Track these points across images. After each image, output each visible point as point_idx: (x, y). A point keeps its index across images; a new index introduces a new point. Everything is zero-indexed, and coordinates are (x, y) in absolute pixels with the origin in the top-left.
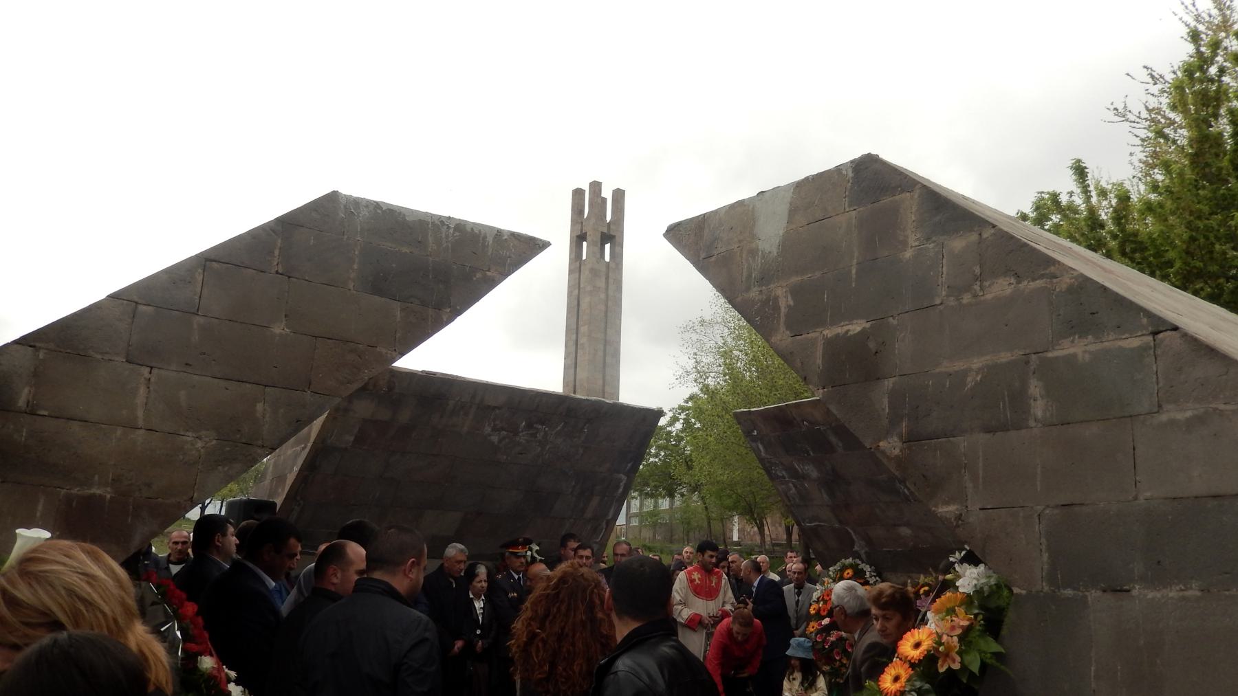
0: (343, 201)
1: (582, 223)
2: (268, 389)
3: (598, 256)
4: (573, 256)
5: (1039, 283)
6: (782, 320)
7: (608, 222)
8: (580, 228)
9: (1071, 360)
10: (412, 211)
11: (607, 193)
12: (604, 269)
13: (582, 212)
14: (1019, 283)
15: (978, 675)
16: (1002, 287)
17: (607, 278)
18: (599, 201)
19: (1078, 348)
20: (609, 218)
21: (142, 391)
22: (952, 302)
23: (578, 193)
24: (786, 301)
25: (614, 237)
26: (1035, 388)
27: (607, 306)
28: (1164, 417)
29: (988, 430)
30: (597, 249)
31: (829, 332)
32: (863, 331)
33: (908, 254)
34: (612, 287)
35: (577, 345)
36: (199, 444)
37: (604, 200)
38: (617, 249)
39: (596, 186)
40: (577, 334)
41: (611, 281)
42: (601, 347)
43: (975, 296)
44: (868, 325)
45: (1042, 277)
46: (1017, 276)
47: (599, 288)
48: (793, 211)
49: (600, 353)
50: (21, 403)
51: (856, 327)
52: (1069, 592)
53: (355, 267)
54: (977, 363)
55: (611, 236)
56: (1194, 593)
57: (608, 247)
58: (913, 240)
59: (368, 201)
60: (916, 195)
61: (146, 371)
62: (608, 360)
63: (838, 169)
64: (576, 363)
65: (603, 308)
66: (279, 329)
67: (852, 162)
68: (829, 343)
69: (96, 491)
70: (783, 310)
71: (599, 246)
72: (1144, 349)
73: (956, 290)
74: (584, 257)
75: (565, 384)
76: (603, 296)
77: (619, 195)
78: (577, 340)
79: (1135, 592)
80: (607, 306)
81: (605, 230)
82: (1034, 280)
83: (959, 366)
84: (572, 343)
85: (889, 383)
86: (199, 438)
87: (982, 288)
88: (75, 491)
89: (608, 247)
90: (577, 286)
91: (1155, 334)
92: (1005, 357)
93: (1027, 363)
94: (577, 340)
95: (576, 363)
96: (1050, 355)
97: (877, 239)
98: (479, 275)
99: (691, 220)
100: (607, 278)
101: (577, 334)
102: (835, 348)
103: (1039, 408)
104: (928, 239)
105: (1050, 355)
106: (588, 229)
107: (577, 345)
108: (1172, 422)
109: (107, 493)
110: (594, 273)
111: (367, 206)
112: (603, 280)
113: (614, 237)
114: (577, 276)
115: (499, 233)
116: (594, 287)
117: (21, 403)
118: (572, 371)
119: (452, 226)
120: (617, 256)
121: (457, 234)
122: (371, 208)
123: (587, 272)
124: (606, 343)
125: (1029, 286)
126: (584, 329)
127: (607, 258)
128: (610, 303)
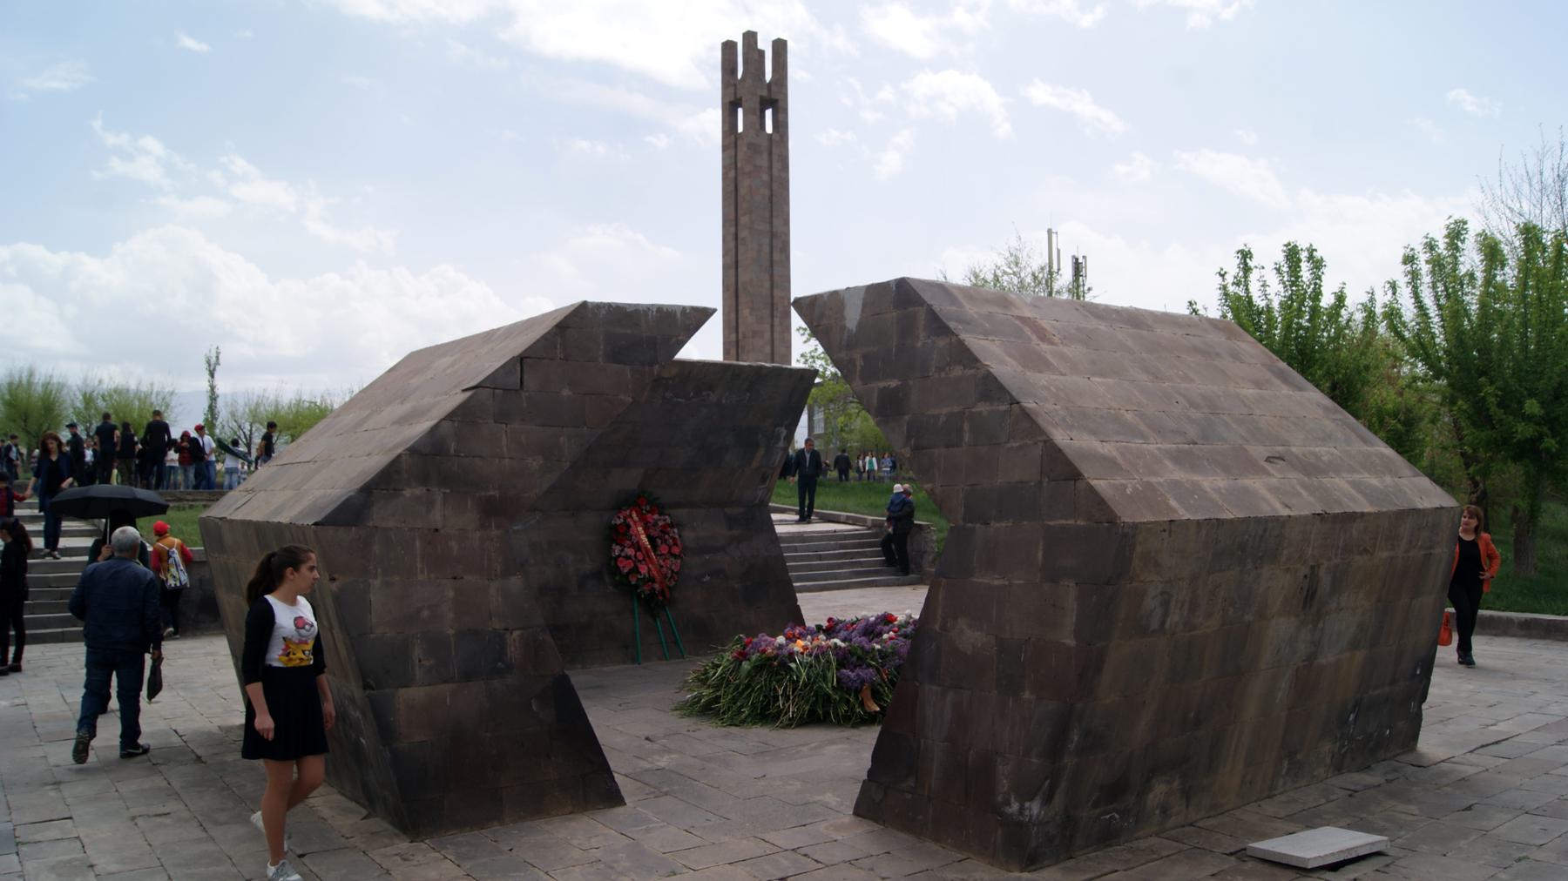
0: (590, 306)
1: (735, 85)
2: (565, 429)
3: (758, 126)
4: (727, 128)
5: (972, 371)
6: (858, 374)
7: (768, 81)
8: (733, 91)
9: (980, 413)
10: (630, 305)
11: (764, 44)
12: (765, 143)
13: (734, 70)
14: (964, 369)
15: (136, 453)
16: (957, 371)
17: (770, 154)
18: (756, 56)
19: (983, 408)
20: (768, 76)
21: (504, 436)
22: (937, 376)
23: (729, 47)
24: (860, 363)
25: (776, 101)
26: (966, 427)
27: (771, 190)
28: (1009, 445)
29: (947, 447)
30: (755, 119)
31: (882, 384)
32: (897, 386)
33: (919, 344)
34: (776, 166)
35: (736, 239)
36: (535, 463)
37: (762, 53)
38: (781, 117)
39: (750, 37)
40: (736, 225)
41: (775, 157)
42: (766, 241)
43: (947, 374)
44: (899, 383)
45: (974, 368)
46: (964, 366)
47: (761, 167)
48: (865, 305)
49: (766, 249)
50: (452, 451)
51: (894, 383)
52: (969, 525)
53: (602, 347)
54: (945, 411)
55: (774, 98)
56: (1010, 524)
57: (769, 113)
58: (922, 335)
59: (604, 304)
60: (925, 308)
61: (504, 426)
62: (776, 257)
63: (888, 283)
64: (737, 262)
65: (767, 192)
66: (566, 392)
67: (896, 280)
68: (882, 391)
69: (492, 493)
70: (859, 368)
71: (758, 113)
72: (1006, 411)
73: (940, 369)
74: (740, 129)
75: (726, 353)
76: (765, 177)
77: (780, 47)
78: (736, 234)
79: (992, 524)
80: (771, 190)
81: (765, 93)
82: (971, 369)
83: (936, 411)
84: (730, 238)
85: (907, 418)
86: (534, 460)
87: (950, 370)
88: (483, 494)
89: (769, 113)
90: (733, 166)
91: (1011, 404)
92: (956, 409)
93: (964, 413)
94: (736, 234)
95: (737, 262)
96: (973, 410)
97: (1083, 106)
98: (674, 340)
99: (808, 297)
100: (770, 154)
101: (736, 225)
102: (884, 393)
103: (967, 437)
104: (929, 337)
105: (973, 410)
106: (742, 93)
107: (736, 239)
108: (1012, 447)
109: (496, 493)
110: (754, 148)
111: (604, 307)
112: (765, 156)
113: (776, 101)
114: (733, 153)
115: (684, 308)
116: (755, 166)
117: (452, 451)
118: (732, 272)
119: (654, 310)
120: (781, 125)
121: (658, 314)
122: (606, 307)
123: (745, 149)
124: (772, 235)
125: (969, 372)
126: (744, 220)
127: (769, 129)
128: (775, 186)
